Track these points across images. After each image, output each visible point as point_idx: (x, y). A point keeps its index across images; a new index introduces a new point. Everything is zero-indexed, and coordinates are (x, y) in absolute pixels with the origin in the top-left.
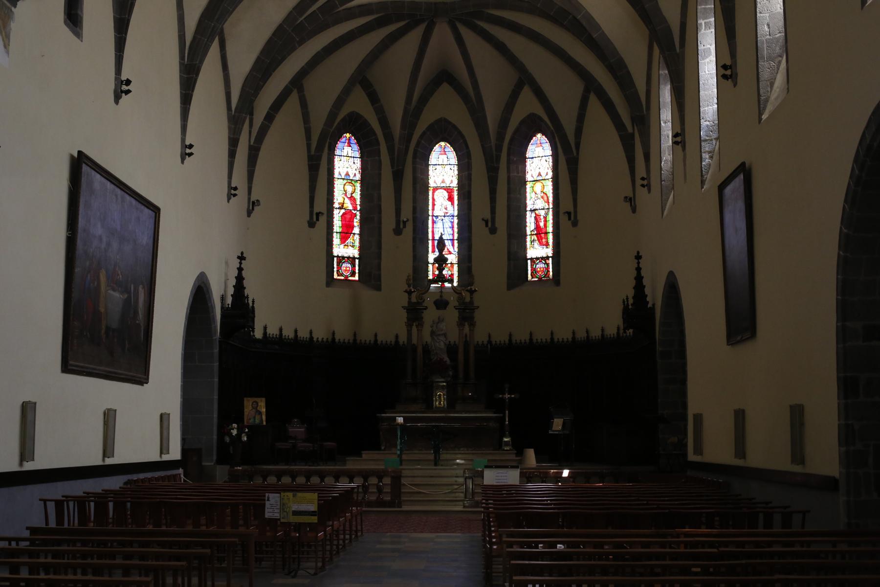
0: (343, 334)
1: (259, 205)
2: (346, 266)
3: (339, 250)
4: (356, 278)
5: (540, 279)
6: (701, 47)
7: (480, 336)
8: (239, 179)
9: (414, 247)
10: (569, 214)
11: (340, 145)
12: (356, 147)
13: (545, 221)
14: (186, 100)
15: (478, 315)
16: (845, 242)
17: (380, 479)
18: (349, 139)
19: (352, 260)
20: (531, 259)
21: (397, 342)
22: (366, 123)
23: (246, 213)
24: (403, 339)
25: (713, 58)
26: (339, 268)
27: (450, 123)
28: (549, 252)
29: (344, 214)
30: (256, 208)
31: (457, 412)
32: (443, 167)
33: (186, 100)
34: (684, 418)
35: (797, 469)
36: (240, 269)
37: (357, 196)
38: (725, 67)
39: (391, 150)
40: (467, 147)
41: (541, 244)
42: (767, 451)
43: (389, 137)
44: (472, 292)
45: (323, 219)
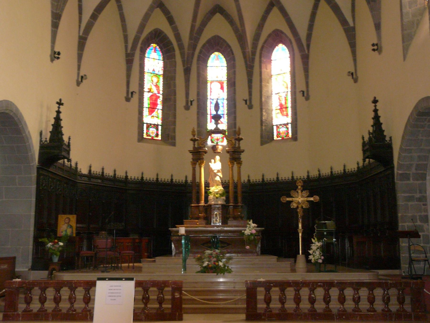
0: (150, 176)
1: (86, 79)
2: (152, 130)
3: (147, 119)
4: (159, 138)
5: (283, 138)
9: (198, 118)
10: (303, 92)
11: (148, 51)
12: (160, 53)
15: (243, 156)
18: (155, 48)
19: (156, 126)
20: (277, 125)
21: (186, 181)
23: (76, 83)
24: (190, 179)
26: (148, 131)
27: (221, 38)
28: (289, 120)
29: (152, 96)
30: (84, 81)
31: (229, 226)
32: (217, 67)
33: (55, 25)
37: (161, 85)
39: (182, 54)
40: (233, 54)
41: (283, 115)
43: (181, 46)
44: (240, 140)
45: (135, 99)
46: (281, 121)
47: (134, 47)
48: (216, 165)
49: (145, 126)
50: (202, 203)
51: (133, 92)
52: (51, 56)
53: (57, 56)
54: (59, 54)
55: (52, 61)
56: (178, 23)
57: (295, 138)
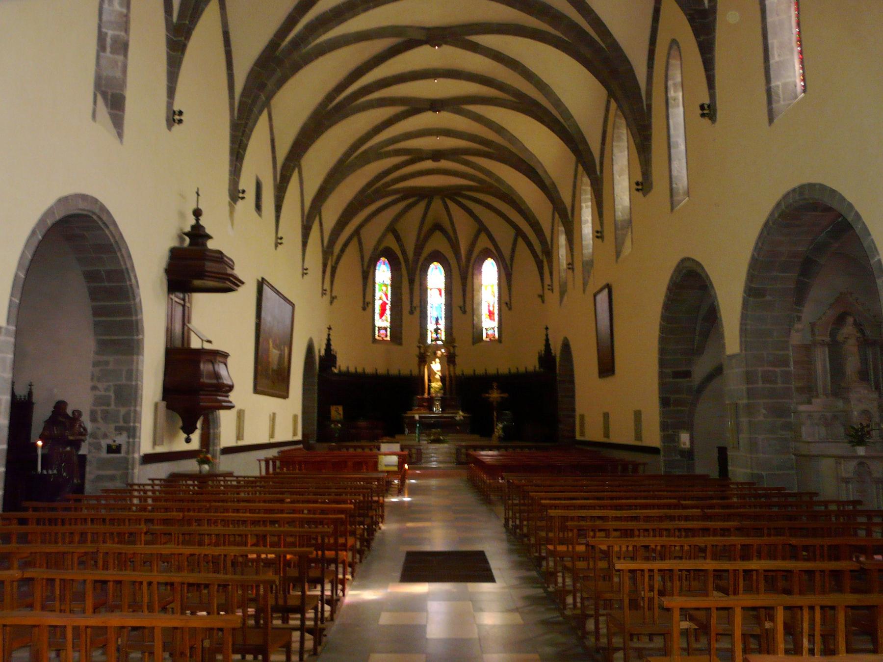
0: (382, 371)
2: (383, 332)
4: (388, 338)
6: (583, 218)
7: (458, 372)
8: (327, 286)
11: (378, 264)
15: (457, 360)
16: (662, 330)
19: (386, 329)
25: (590, 225)
32: (436, 276)
33: (305, 244)
34: (574, 417)
36: (329, 335)
38: (598, 232)
43: (406, 260)
44: (454, 347)
46: (489, 326)
48: (436, 366)
49: (377, 329)
50: (426, 396)
51: (367, 304)
52: (167, 121)
53: (177, 117)
54: (181, 113)
57: (500, 340)
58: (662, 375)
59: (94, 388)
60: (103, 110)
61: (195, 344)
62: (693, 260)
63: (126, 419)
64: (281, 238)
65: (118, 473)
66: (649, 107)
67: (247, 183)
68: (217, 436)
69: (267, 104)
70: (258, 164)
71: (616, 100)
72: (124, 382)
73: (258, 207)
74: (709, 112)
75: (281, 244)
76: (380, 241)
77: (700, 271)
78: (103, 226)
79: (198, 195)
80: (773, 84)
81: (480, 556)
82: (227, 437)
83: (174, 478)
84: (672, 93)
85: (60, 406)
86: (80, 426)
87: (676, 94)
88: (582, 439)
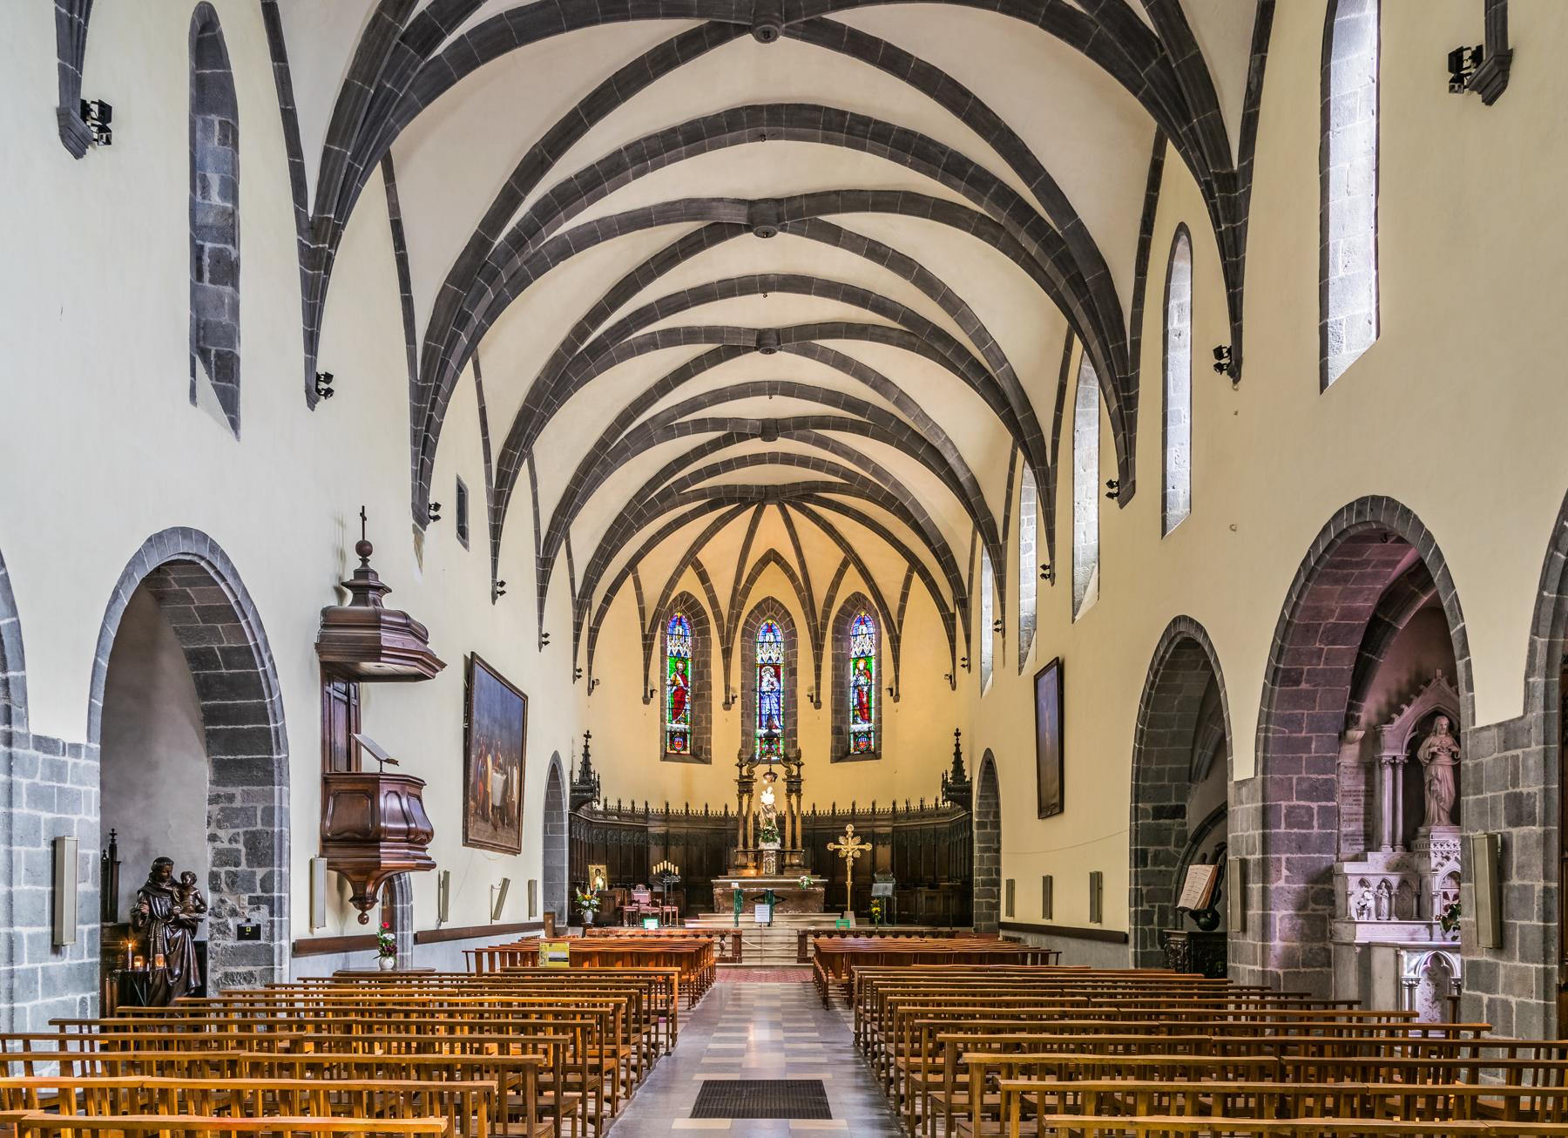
8: (582, 662)
13: (869, 697)
14: (542, 591)
17: (723, 937)
22: (696, 603)
33: (542, 591)
34: (997, 883)
35: (1096, 926)
36: (586, 747)
38: (1044, 567)
39: (720, 628)
42: (1072, 910)
47: (653, 628)
52: (308, 392)
53: (323, 386)
55: (312, 404)
56: (713, 580)
58: (1136, 813)
59: (213, 838)
60: (205, 382)
61: (369, 765)
62: (1192, 621)
63: (267, 883)
64: (502, 584)
65: (256, 970)
66: (1136, 344)
67: (442, 491)
68: (408, 914)
69: (471, 350)
70: (461, 455)
71: (1082, 336)
72: (259, 827)
73: (462, 532)
74: (1229, 361)
75: (502, 593)
76: (671, 584)
77: (1200, 639)
78: (216, 578)
79: (364, 519)
80: (1331, 320)
81: (817, 1087)
82: (423, 916)
83: (343, 978)
84: (1174, 324)
85: (161, 869)
86: (196, 896)
87: (1180, 323)
88: (1009, 920)
